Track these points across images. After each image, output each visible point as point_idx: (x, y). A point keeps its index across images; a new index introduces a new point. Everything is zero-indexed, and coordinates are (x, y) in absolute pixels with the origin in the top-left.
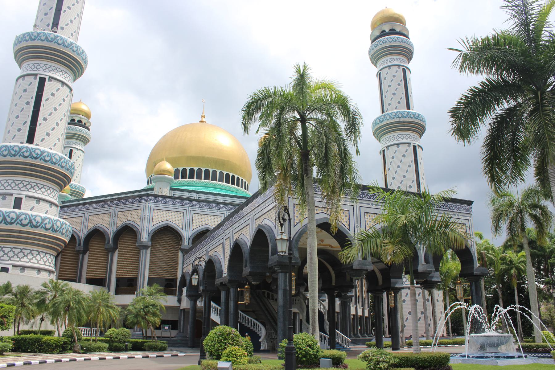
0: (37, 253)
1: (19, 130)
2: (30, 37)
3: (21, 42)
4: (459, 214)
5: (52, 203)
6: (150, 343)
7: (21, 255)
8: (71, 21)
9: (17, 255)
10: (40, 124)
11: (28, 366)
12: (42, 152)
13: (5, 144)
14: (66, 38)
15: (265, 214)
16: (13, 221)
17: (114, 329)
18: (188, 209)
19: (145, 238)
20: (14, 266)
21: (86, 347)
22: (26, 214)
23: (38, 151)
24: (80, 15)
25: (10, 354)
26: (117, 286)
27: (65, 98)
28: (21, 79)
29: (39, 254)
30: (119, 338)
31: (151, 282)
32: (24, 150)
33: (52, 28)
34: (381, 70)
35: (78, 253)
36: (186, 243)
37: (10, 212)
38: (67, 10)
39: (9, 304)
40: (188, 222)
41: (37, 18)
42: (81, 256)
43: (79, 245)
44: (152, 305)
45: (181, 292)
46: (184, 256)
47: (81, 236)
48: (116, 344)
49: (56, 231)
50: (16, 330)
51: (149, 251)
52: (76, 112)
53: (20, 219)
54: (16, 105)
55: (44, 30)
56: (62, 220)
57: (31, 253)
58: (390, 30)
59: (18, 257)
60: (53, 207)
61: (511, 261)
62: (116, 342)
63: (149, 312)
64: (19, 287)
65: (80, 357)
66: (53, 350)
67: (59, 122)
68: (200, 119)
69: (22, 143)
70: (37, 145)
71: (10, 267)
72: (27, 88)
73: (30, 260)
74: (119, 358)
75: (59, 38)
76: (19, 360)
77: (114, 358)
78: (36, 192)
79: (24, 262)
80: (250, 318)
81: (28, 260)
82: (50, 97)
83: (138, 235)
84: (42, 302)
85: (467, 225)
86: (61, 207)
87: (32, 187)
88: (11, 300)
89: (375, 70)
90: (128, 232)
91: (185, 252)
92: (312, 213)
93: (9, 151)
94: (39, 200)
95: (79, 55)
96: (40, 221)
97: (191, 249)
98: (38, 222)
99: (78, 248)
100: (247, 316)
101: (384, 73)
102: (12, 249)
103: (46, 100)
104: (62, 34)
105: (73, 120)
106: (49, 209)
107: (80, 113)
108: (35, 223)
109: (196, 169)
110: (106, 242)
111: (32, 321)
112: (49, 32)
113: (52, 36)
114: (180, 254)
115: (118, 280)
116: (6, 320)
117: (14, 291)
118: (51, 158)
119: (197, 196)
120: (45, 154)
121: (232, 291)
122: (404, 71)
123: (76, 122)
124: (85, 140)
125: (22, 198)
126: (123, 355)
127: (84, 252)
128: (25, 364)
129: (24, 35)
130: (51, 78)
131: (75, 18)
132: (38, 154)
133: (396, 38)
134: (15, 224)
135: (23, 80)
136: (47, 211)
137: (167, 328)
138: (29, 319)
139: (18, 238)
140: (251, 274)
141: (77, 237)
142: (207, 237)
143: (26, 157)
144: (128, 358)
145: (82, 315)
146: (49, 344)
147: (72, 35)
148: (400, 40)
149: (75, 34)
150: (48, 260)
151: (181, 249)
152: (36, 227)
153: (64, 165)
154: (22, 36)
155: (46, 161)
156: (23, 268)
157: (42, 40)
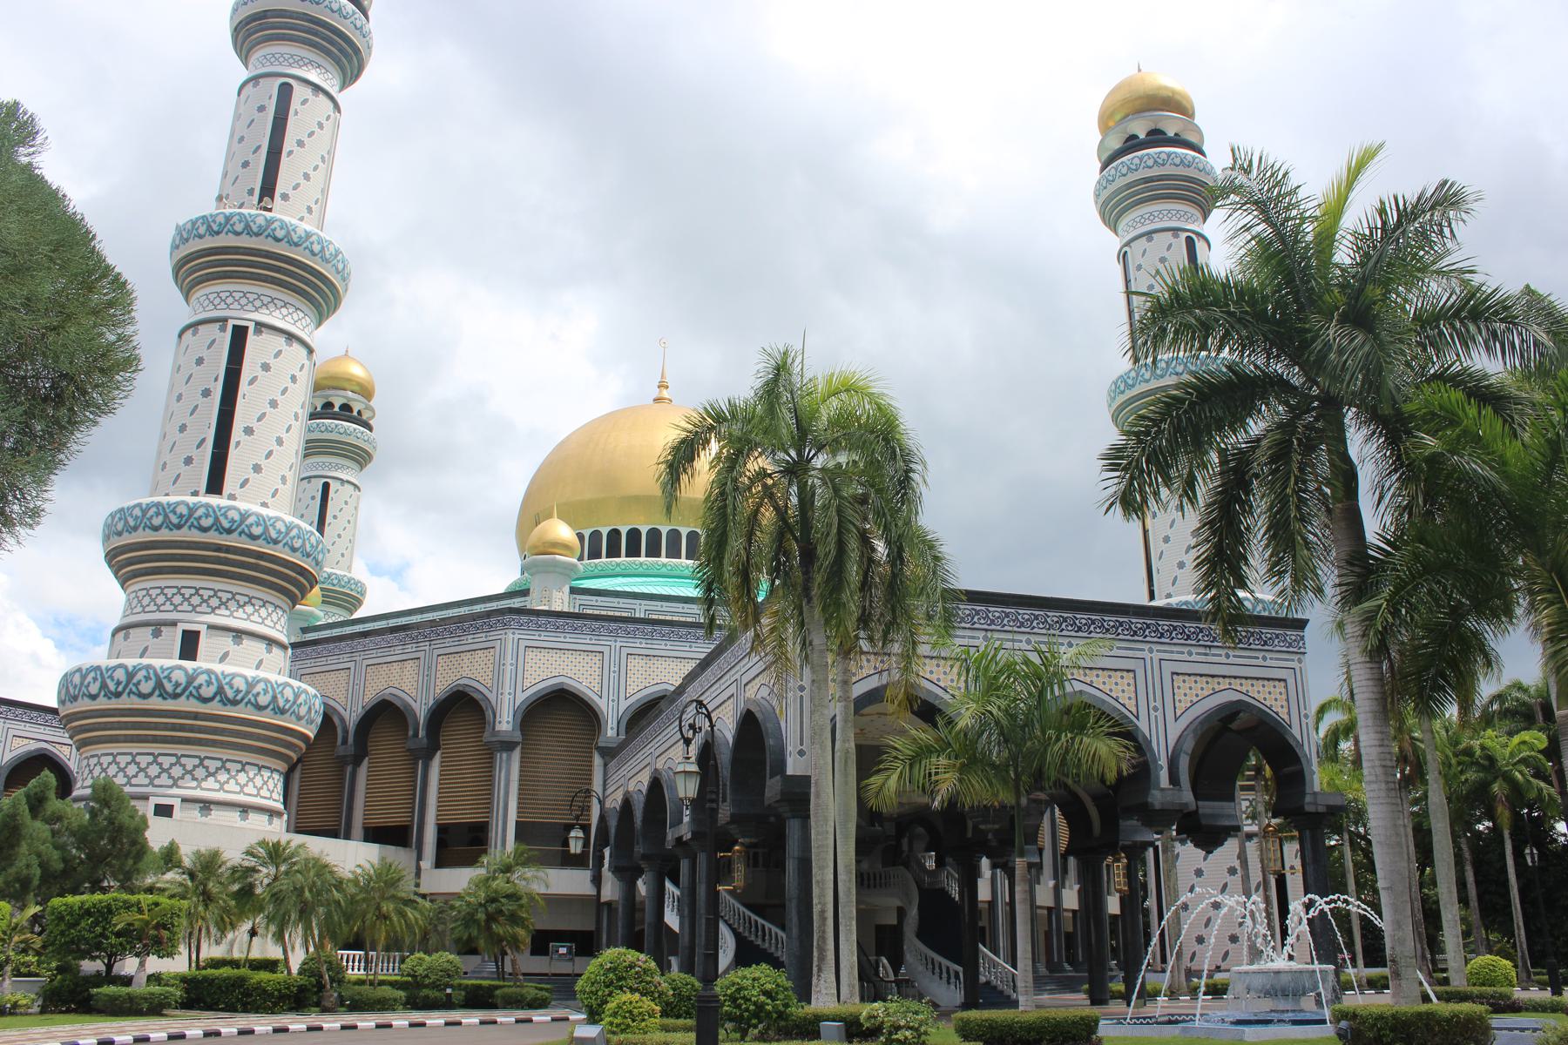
0: (239, 766)
1: (188, 461)
2: (209, 227)
3: (187, 240)
4: (1268, 655)
5: (271, 642)
6: (509, 989)
7: (200, 773)
8: (307, 177)
9: (190, 772)
10: (238, 443)
11: (213, 1039)
12: (244, 516)
13: (156, 499)
14: (295, 221)
15: (741, 685)
16: (179, 690)
17: (421, 955)
18: (613, 645)
19: (505, 722)
20: (185, 800)
21: (352, 1000)
22: (209, 672)
23: (233, 514)
24: (328, 159)
25: (178, 1012)
26: (441, 844)
27: (298, 374)
28: (122, 634)
29: (243, 770)
30: (433, 977)
31: (523, 831)
32: (201, 512)
33: (260, 200)
34: (1127, 244)
35: (342, 762)
36: (611, 731)
37: (172, 669)
38: (296, 149)
39: (172, 897)
40: (614, 678)
41: (225, 175)
42: (349, 769)
43: (345, 741)
44: (508, 896)
45: (600, 860)
46: (605, 765)
47: (347, 718)
48: (425, 992)
49: (283, 712)
50: (194, 957)
51: (516, 755)
52: (335, 384)
53: (196, 684)
54: (179, 398)
55: (241, 207)
56: (295, 683)
57: (223, 767)
58: (1150, 133)
59: (194, 779)
60: (275, 650)
61: (1491, 760)
62: (426, 986)
63: (500, 912)
64: (198, 854)
65: (331, 1023)
66: (275, 1004)
67: (284, 436)
68: (655, 393)
69: (195, 494)
70: (232, 497)
71: (176, 803)
72: (205, 354)
73: (222, 785)
74: (423, 1025)
75: (276, 225)
76: (194, 1026)
77: (411, 1025)
78: (231, 615)
79: (209, 789)
80: (767, 925)
81: (217, 786)
82: (260, 373)
83: (489, 714)
84: (246, 893)
85: (1291, 682)
86: (294, 646)
87: (224, 604)
88: (181, 884)
89: (1113, 243)
90: (462, 706)
91: (609, 754)
92: (819, 689)
93: (166, 516)
94: (239, 634)
95: (328, 261)
96: (243, 687)
97: (622, 746)
98: (238, 691)
99: (341, 750)
100: (760, 921)
101: (1134, 252)
102: (179, 758)
103: (251, 382)
104: (284, 213)
105: (329, 405)
106: (265, 656)
107: (346, 385)
108: (230, 694)
109: (644, 530)
110: (411, 733)
111: (230, 936)
112: (254, 212)
113: (260, 221)
114: (597, 761)
115: (443, 830)
116: (165, 934)
117: (187, 862)
118: (266, 528)
119: (640, 610)
120: (251, 520)
121: (702, 859)
122: (1190, 243)
123: (336, 409)
124: (360, 457)
125: (198, 633)
126: (436, 1019)
127: (357, 761)
128: (207, 1035)
129: (194, 223)
130: (260, 326)
131: (316, 168)
132: (233, 521)
133: (1164, 156)
134: (183, 698)
135: (126, 638)
136: (261, 662)
137: (563, 951)
138: (223, 931)
139: (192, 731)
140: (735, 819)
141: (336, 720)
142: (661, 712)
143: (205, 530)
144: (447, 1024)
145: (352, 918)
146: (265, 991)
147: (310, 210)
148: (1177, 161)
149: (317, 208)
150: (265, 783)
151: (598, 748)
152: (235, 703)
153: (298, 543)
154: (189, 226)
155: (254, 538)
156: (206, 805)
157: (237, 234)
